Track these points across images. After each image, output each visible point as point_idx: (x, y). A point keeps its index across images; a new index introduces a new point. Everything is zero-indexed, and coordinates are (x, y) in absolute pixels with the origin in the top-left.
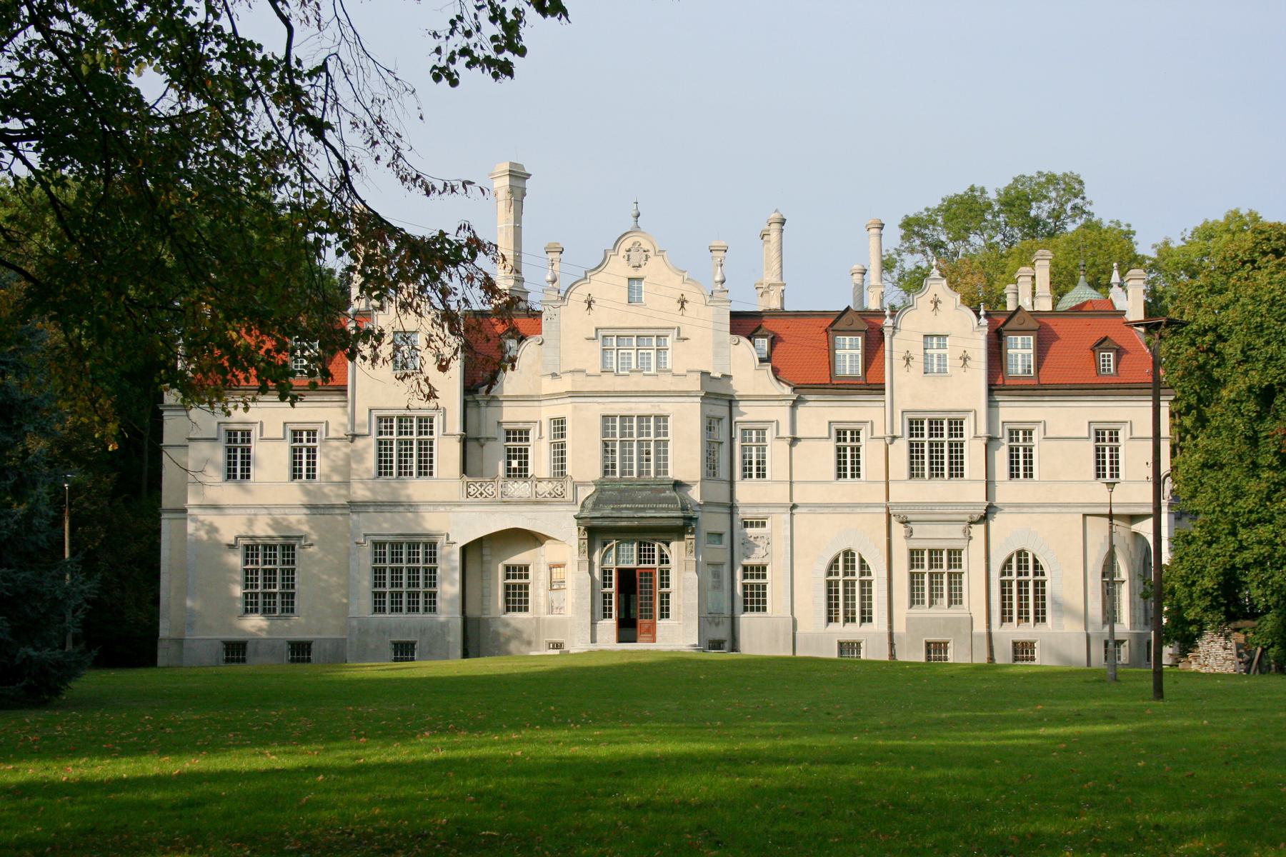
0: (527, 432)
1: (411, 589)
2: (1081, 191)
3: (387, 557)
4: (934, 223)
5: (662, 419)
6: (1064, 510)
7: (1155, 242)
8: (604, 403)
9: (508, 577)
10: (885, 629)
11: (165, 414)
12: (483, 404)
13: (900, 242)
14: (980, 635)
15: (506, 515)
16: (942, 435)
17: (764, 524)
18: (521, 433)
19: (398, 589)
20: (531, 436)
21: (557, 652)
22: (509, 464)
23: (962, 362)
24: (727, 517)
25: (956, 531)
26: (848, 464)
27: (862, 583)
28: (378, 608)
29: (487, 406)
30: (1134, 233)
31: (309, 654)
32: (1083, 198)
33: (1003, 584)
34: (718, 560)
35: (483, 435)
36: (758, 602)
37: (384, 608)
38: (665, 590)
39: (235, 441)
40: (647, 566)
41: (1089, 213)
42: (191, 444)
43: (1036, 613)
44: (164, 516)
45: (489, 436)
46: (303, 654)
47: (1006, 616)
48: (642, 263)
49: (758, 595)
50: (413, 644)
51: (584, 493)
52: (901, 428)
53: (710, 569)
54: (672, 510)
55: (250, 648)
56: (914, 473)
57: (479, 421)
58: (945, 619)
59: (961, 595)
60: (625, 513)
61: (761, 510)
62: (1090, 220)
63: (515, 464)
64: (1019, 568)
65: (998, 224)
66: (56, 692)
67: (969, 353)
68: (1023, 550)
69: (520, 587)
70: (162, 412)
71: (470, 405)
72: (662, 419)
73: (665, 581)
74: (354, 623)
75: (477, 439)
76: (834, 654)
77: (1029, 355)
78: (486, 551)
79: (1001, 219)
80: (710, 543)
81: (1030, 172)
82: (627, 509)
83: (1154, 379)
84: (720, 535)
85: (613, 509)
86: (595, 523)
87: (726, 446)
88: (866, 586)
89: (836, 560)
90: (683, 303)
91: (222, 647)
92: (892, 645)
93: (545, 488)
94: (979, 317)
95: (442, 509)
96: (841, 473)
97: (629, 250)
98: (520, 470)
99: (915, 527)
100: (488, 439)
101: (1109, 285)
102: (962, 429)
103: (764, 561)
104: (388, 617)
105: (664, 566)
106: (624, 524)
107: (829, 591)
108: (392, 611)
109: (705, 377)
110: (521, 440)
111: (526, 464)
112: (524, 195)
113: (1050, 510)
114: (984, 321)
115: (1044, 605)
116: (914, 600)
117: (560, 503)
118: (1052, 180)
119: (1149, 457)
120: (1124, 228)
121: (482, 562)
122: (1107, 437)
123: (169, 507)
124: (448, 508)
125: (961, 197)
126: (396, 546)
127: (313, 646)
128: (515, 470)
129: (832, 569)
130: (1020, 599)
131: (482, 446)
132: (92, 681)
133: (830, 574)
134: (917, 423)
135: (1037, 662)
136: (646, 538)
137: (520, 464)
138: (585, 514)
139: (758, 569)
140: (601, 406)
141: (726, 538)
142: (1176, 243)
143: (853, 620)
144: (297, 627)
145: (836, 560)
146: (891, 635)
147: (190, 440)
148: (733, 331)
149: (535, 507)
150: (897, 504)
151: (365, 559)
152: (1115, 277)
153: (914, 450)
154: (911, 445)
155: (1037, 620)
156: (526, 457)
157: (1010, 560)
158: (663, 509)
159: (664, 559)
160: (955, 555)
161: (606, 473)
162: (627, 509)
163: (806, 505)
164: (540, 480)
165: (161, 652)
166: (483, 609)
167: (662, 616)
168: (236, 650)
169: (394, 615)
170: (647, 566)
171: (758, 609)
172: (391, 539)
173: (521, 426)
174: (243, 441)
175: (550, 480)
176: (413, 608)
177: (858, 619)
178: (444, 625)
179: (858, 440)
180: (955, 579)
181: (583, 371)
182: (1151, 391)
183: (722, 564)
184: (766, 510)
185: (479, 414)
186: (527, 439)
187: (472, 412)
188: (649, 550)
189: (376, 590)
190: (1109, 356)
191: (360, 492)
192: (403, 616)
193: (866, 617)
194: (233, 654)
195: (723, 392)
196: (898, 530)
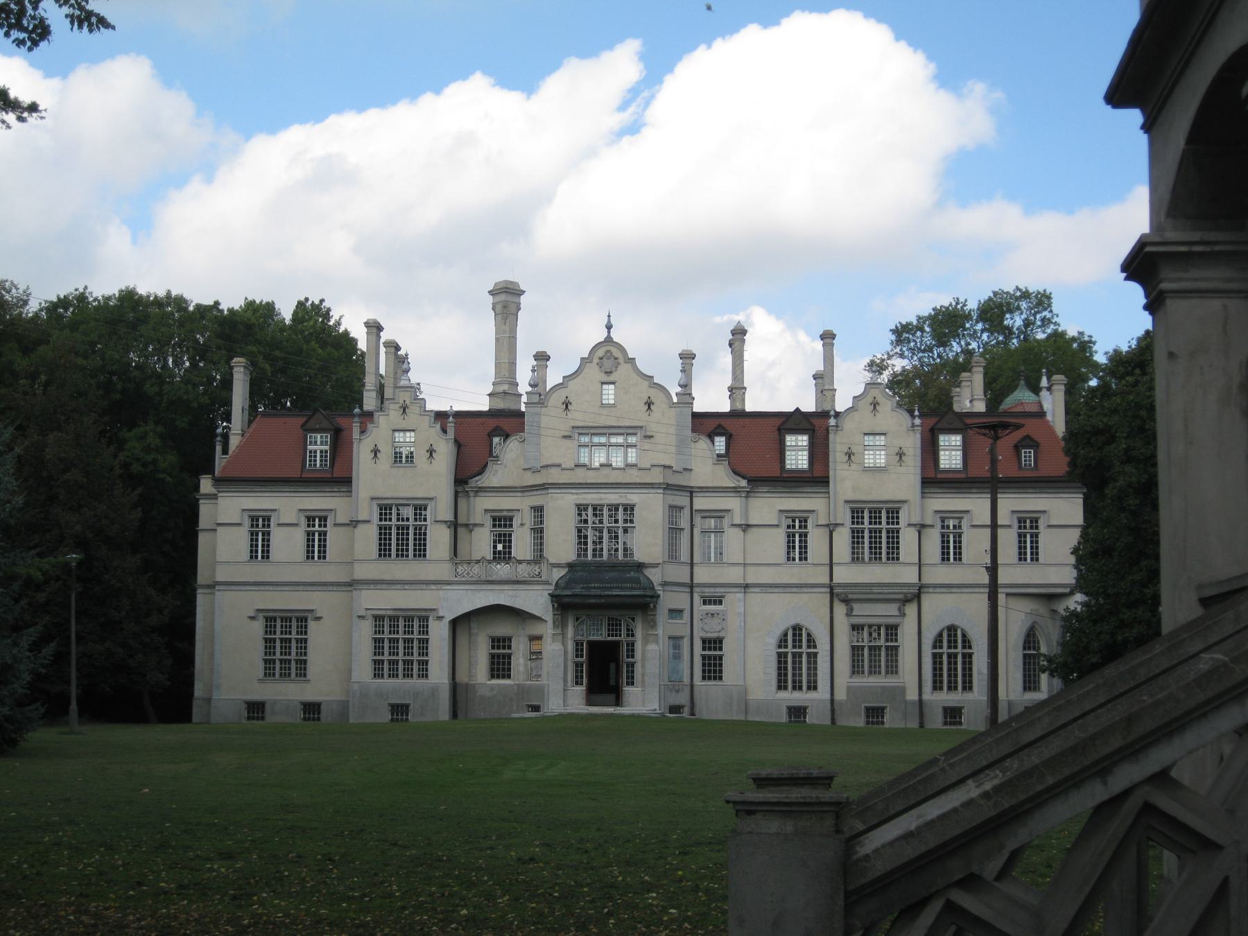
0: (511, 519)
1: (407, 658)
2: (1049, 305)
3: (415, 629)
4: (922, 330)
5: (629, 509)
6: (309, 588)
7: (1107, 350)
8: (577, 494)
9: (704, 649)
10: (828, 696)
11: (201, 502)
12: (472, 494)
13: (889, 348)
14: (912, 702)
15: (490, 593)
16: (880, 523)
17: (720, 603)
18: (505, 519)
19: (395, 658)
20: (514, 523)
21: (534, 714)
22: (495, 547)
23: (898, 458)
24: (688, 596)
25: (892, 609)
26: (797, 545)
27: (964, 655)
28: (378, 674)
29: (475, 496)
30: (1094, 343)
31: (319, 713)
32: (1051, 311)
33: (935, 656)
34: (678, 634)
35: (472, 522)
36: (715, 671)
37: (412, 675)
38: (631, 660)
39: (257, 526)
40: (614, 638)
41: (1056, 324)
42: (219, 529)
43: (949, 682)
44: (199, 591)
45: (476, 522)
46: (314, 714)
47: (937, 686)
48: (614, 369)
49: (715, 665)
50: (407, 706)
51: (558, 574)
52: (844, 516)
53: (671, 642)
54: (635, 589)
55: (268, 708)
56: (856, 558)
57: (469, 510)
58: (882, 687)
59: (704, 665)
60: (593, 592)
61: (718, 590)
62: (1057, 329)
63: (500, 547)
64: (949, 641)
65: (975, 331)
66: (13, 743)
67: (905, 450)
68: (798, 625)
69: (715, 657)
70: (198, 500)
71: (460, 495)
72: (629, 509)
73: (631, 652)
74: (356, 687)
75: (467, 525)
76: (784, 718)
77: (326, 452)
78: (474, 625)
79: (979, 326)
80: (672, 618)
81: (1010, 288)
82: (595, 588)
83: (992, 475)
84: (681, 611)
85: (583, 588)
86: (567, 600)
87: (687, 532)
88: (813, 657)
89: (786, 635)
90: (649, 404)
91: (244, 706)
92: (833, 711)
93: (523, 571)
94: (913, 416)
95: (433, 587)
96: (309, 555)
97: (601, 359)
98: (505, 553)
99: (856, 606)
100: (475, 525)
101: (1040, 389)
102: (898, 518)
103: (721, 635)
104: (387, 682)
105: (630, 638)
106: (593, 601)
107: (779, 662)
108: (389, 676)
109: (667, 471)
110: (505, 526)
111: (510, 547)
112: (519, 309)
113: (977, 590)
114: (917, 421)
115: (971, 676)
116: (856, 669)
117: (538, 583)
118: (1026, 295)
119: (987, 545)
120: (1086, 338)
121: (470, 634)
122: (1028, 524)
123: (203, 583)
124: (439, 586)
125: (947, 308)
126: (394, 619)
127: (323, 707)
128: (500, 552)
129: (782, 642)
130: (809, 669)
131: (471, 531)
132: (42, 736)
133: (780, 647)
134: (858, 512)
135: (887, 726)
136: (615, 614)
137: (504, 547)
138: (558, 592)
139: (715, 642)
140: (575, 496)
141: (687, 614)
142: (1125, 348)
143: (941, 688)
144: (307, 692)
145: (786, 635)
146: (832, 701)
147: (219, 524)
148: (693, 431)
149: (515, 587)
150: (840, 585)
151: (365, 631)
152: (1044, 382)
153: (856, 536)
154: (853, 532)
155: (964, 688)
156: (510, 541)
157: (940, 635)
158: (627, 588)
159: (631, 633)
160: (892, 630)
161: (579, 555)
162: (595, 588)
163: (936, 586)
164: (520, 562)
165: (195, 710)
166: (470, 676)
167: (628, 684)
168: (256, 709)
169: (391, 680)
170: (614, 638)
171: (715, 678)
172: (389, 613)
173: (505, 513)
174: (264, 526)
175: (529, 562)
176: (408, 674)
177: (805, 687)
178: (434, 690)
179: (806, 527)
180: (893, 651)
181: (559, 466)
182: (989, 485)
183: (682, 638)
184: (723, 590)
185: (468, 505)
186: (511, 526)
187: (462, 503)
188: (616, 625)
189: (375, 658)
190: (1030, 452)
191: (361, 572)
192: (400, 681)
193: (813, 686)
194: (253, 713)
195: (685, 484)
196: (840, 609)
